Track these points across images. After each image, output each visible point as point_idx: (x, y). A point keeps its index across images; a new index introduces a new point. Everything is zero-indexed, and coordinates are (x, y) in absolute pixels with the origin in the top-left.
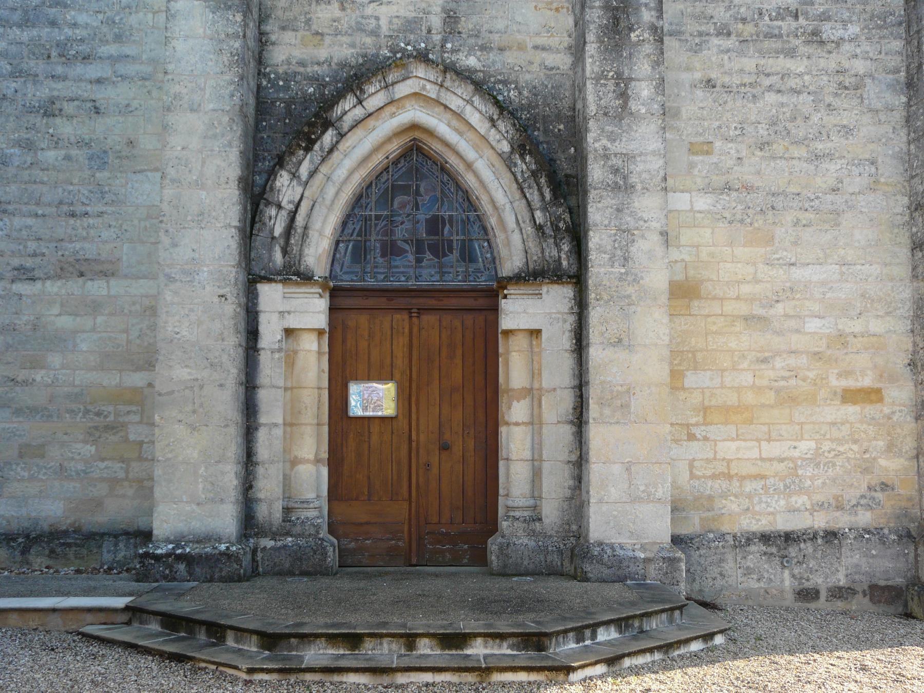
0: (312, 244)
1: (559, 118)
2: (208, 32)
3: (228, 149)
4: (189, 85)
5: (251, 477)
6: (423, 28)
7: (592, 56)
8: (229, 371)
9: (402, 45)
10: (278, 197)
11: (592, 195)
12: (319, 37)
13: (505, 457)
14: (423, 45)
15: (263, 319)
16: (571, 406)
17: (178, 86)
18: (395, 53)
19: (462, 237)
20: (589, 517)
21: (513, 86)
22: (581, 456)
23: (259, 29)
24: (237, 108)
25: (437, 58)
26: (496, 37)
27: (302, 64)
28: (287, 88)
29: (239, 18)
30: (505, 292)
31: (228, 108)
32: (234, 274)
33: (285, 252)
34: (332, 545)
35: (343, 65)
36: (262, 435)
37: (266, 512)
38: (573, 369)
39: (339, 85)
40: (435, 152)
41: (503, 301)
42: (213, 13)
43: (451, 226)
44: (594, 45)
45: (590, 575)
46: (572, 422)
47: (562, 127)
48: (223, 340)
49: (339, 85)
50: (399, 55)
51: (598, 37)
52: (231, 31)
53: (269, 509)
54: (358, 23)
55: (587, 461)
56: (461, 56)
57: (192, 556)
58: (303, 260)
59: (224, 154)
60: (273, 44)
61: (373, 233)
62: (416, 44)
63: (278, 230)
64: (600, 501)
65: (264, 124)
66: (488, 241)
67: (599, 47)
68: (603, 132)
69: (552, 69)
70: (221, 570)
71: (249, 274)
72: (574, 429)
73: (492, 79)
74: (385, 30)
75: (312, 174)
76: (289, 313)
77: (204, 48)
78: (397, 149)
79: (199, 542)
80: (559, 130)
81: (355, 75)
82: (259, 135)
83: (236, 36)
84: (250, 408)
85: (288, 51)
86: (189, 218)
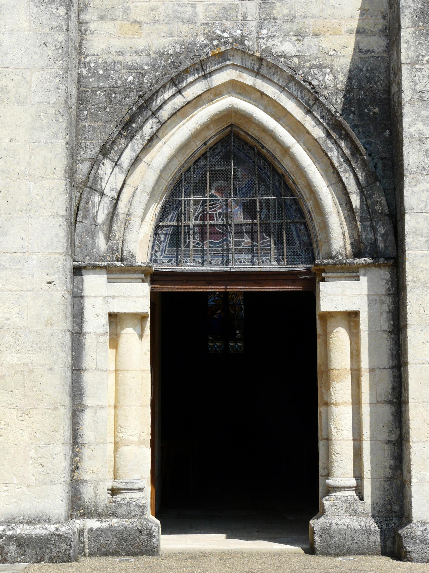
0: (134, 230)
1: (374, 101)
2: (33, 25)
3: (54, 140)
4: (15, 78)
5: (78, 458)
6: (239, 15)
7: (407, 42)
8: (58, 356)
9: (219, 32)
10: (101, 185)
11: (407, 180)
12: (137, 26)
13: (324, 437)
14: (239, 32)
15: (87, 303)
16: (390, 386)
17: (5, 79)
18: (211, 40)
19: (279, 221)
20: (411, 496)
21: (328, 70)
22: (401, 434)
23: (79, 19)
24: (62, 100)
25: (253, 44)
26: (310, 21)
27: (122, 53)
28: (107, 77)
29: (62, 11)
30: (323, 275)
31: (54, 100)
32: (62, 261)
33: (108, 238)
34: (157, 526)
35: (161, 54)
36: (87, 418)
37: (92, 494)
38: (391, 350)
39: (158, 73)
40: (252, 137)
41: (321, 283)
42: (37, 7)
43: (269, 210)
44: (409, 30)
45: (413, 555)
46: (390, 402)
47: (377, 110)
48: (52, 325)
49: (158, 73)
50: (215, 43)
51: (413, 22)
52: (55, 24)
53: (96, 492)
54: (174, 11)
55: (408, 441)
56: (276, 41)
57: (22, 537)
58: (125, 246)
59: (50, 145)
60: (93, 33)
61: (193, 218)
62: (232, 31)
63: (101, 217)
64: (422, 481)
65: (86, 113)
66: (305, 224)
67: (414, 32)
68: (418, 116)
69: (366, 52)
70: (51, 551)
71: (75, 261)
72: (393, 409)
73: (308, 64)
74: (201, 18)
75: (136, 161)
76: (113, 297)
77: (29, 42)
78: (215, 135)
79: (29, 523)
80: (374, 113)
81: (173, 62)
82: (81, 124)
83: (60, 29)
84: (77, 391)
85: (105, 41)
86: (18, 207)
